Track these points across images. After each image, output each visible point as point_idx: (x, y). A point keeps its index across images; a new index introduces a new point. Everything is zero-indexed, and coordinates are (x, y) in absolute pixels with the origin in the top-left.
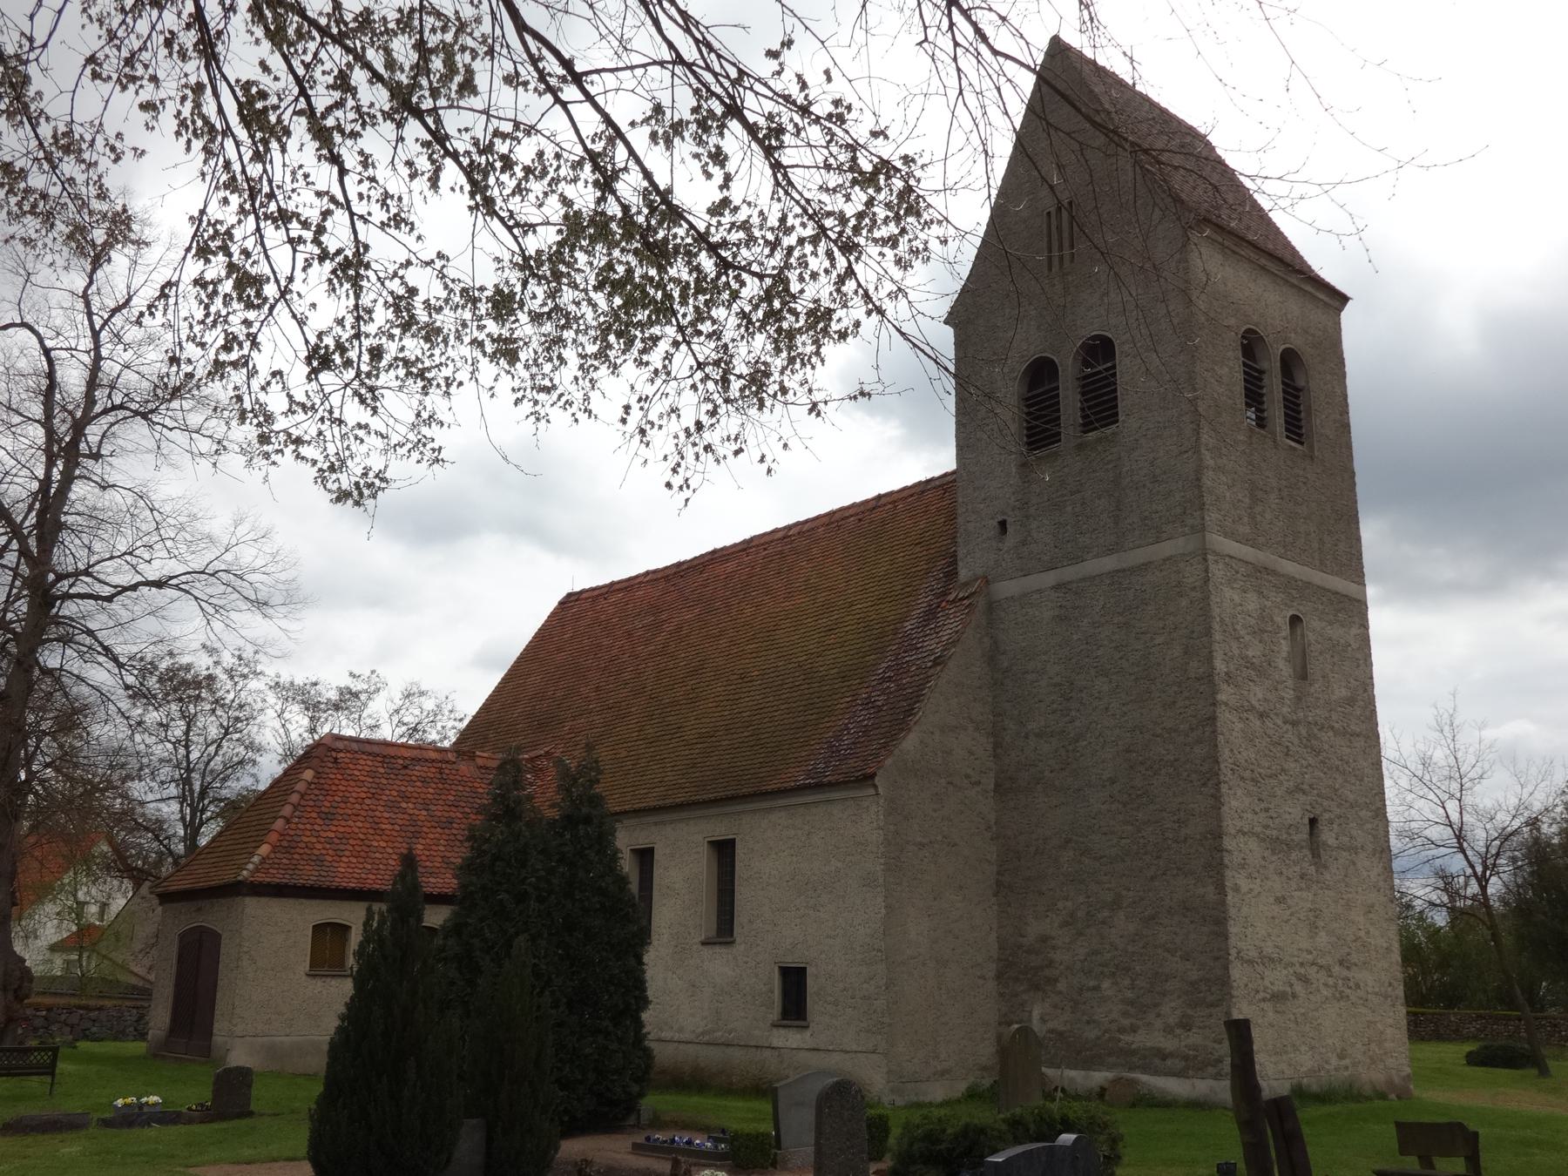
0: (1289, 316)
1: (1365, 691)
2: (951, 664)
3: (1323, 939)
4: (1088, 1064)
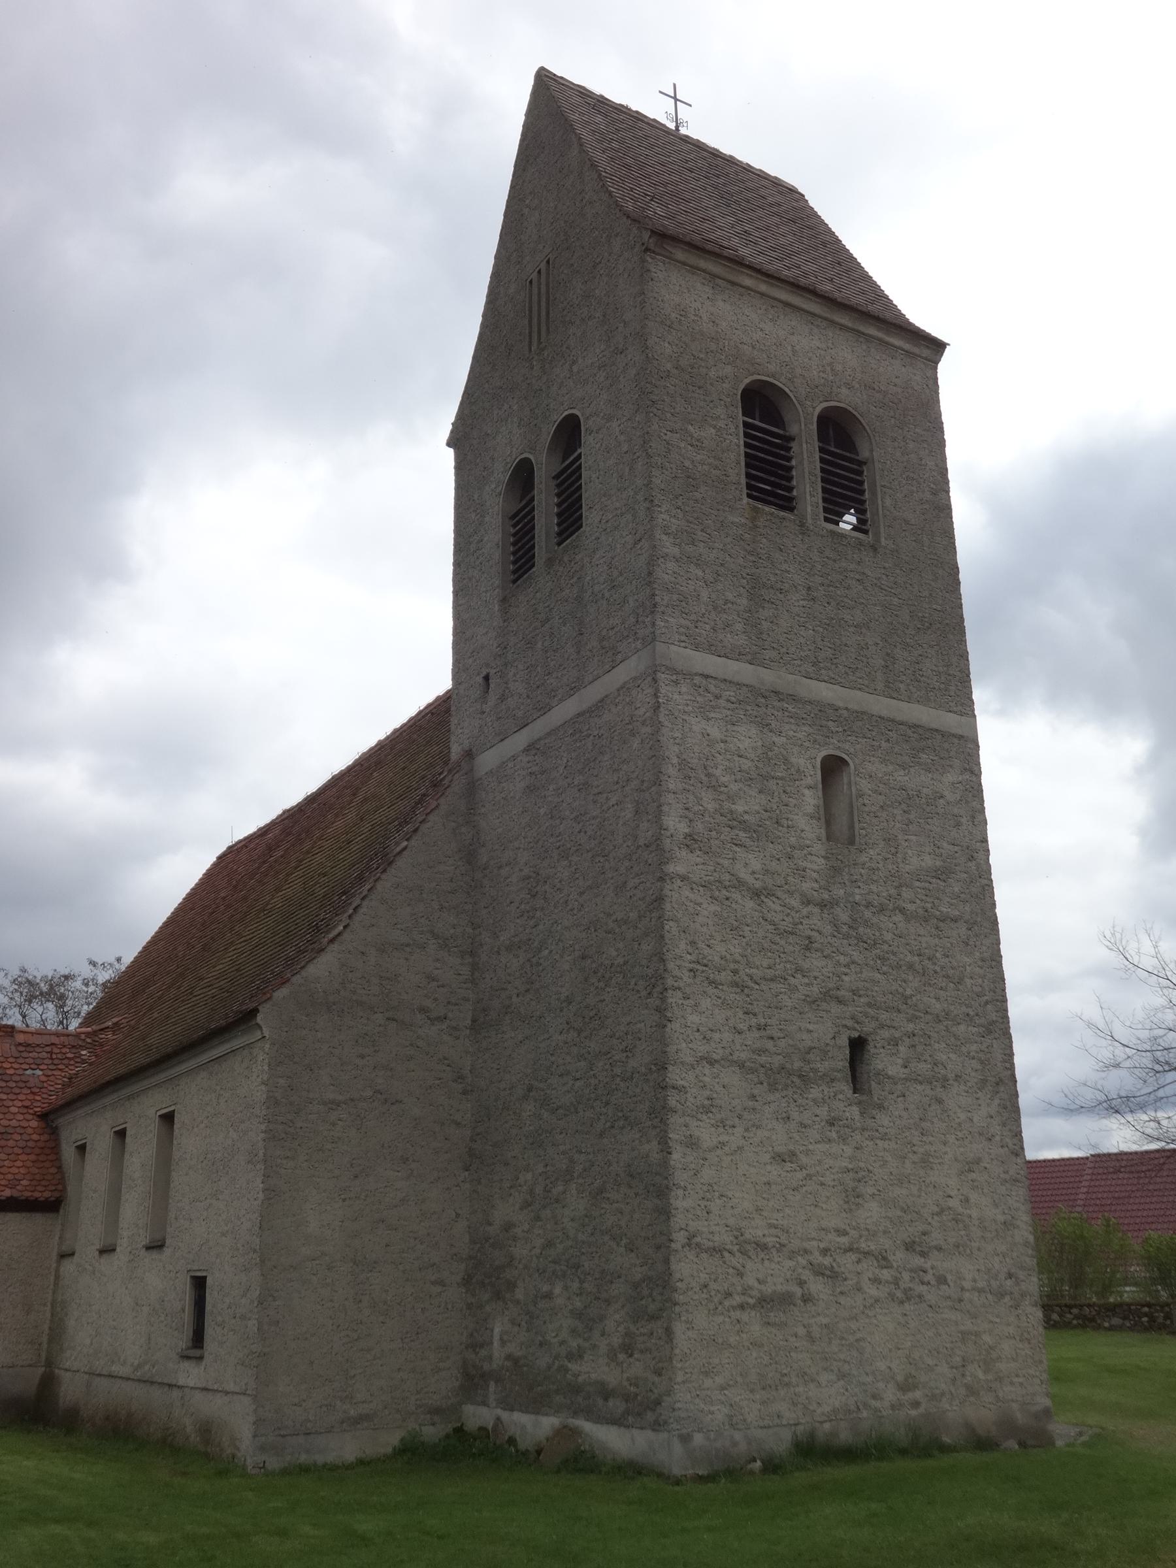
0: (839, 368)
1: (972, 858)
2: (400, 862)
3: (872, 1212)
4: (537, 1405)
